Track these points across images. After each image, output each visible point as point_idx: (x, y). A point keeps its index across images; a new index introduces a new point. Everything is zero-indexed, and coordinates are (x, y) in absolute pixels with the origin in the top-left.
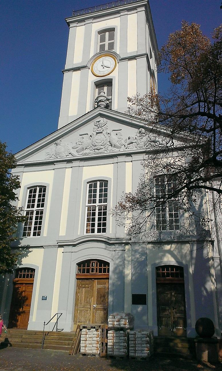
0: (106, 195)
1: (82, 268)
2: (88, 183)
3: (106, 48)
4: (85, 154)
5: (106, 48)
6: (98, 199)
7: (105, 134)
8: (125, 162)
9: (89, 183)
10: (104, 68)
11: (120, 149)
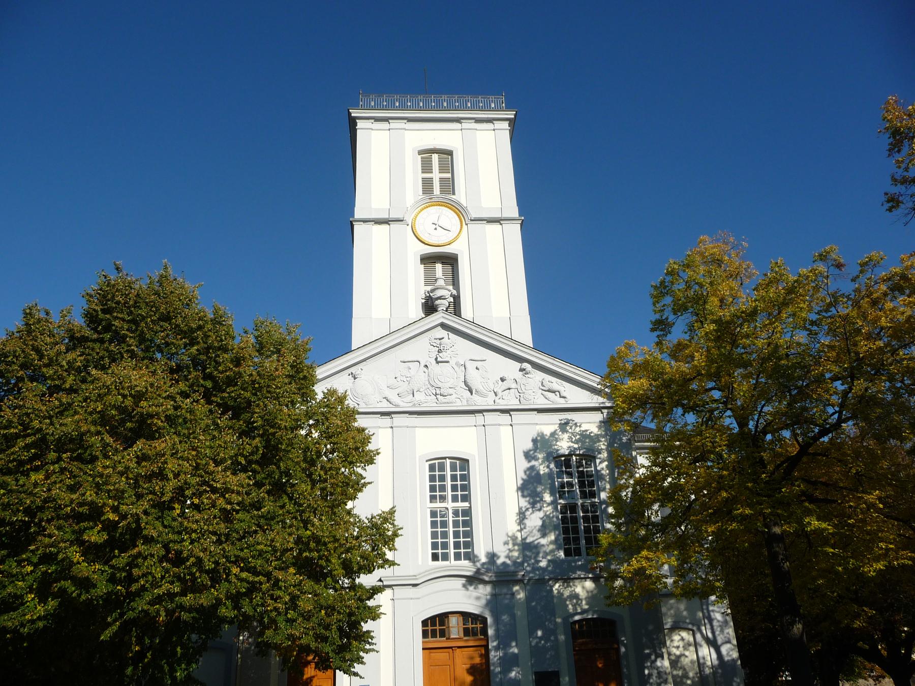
0: (466, 488)
1: (430, 628)
6: (449, 493)
7: (455, 367)
8: (499, 425)
10: (436, 229)
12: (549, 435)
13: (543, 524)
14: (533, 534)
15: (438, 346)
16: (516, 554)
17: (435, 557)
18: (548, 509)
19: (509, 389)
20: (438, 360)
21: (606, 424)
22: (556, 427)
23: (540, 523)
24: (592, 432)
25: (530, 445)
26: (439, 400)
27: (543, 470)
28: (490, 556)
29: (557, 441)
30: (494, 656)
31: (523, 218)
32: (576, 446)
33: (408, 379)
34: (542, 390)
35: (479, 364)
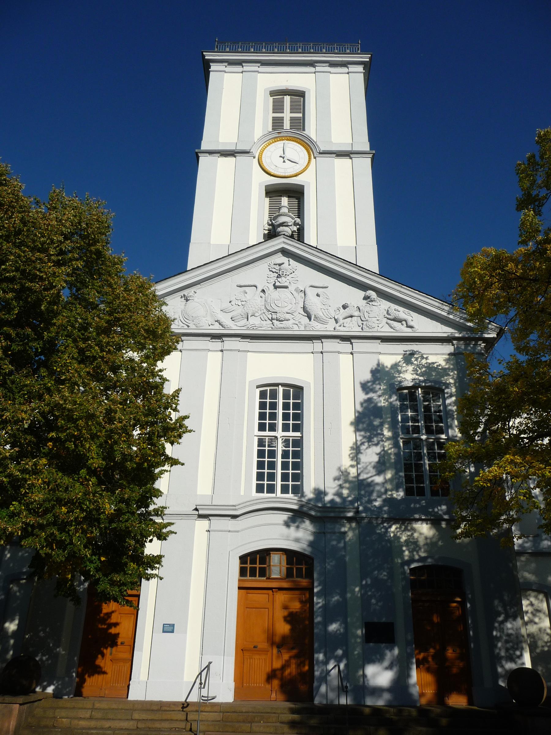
0: (298, 417)
1: (248, 566)
2: (258, 387)
3: (287, 125)
4: (254, 327)
5: (287, 125)
6: (280, 422)
7: (294, 293)
8: (339, 353)
9: (260, 387)
11: (325, 326)
12: (389, 366)
13: (379, 460)
14: (367, 471)
15: (278, 271)
16: (345, 492)
17: (260, 489)
18: (387, 445)
19: (351, 316)
20: (276, 284)
21: (455, 355)
22: (399, 358)
23: (376, 459)
24: (440, 365)
25: (368, 376)
26: (275, 325)
27: (382, 402)
28: (317, 492)
29: (400, 374)
30: (319, 602)
31: (374, 152)
32: (421, 378)
33: (243, 303)
34: (388, 319)
35: (320, 291)
